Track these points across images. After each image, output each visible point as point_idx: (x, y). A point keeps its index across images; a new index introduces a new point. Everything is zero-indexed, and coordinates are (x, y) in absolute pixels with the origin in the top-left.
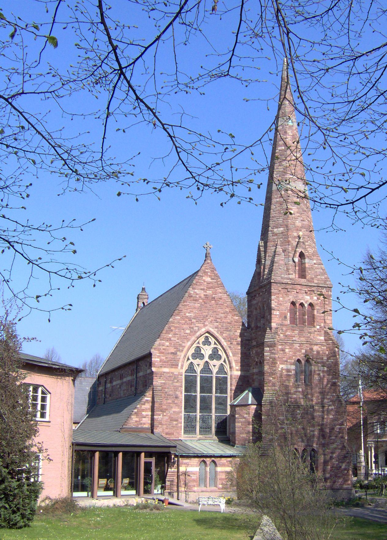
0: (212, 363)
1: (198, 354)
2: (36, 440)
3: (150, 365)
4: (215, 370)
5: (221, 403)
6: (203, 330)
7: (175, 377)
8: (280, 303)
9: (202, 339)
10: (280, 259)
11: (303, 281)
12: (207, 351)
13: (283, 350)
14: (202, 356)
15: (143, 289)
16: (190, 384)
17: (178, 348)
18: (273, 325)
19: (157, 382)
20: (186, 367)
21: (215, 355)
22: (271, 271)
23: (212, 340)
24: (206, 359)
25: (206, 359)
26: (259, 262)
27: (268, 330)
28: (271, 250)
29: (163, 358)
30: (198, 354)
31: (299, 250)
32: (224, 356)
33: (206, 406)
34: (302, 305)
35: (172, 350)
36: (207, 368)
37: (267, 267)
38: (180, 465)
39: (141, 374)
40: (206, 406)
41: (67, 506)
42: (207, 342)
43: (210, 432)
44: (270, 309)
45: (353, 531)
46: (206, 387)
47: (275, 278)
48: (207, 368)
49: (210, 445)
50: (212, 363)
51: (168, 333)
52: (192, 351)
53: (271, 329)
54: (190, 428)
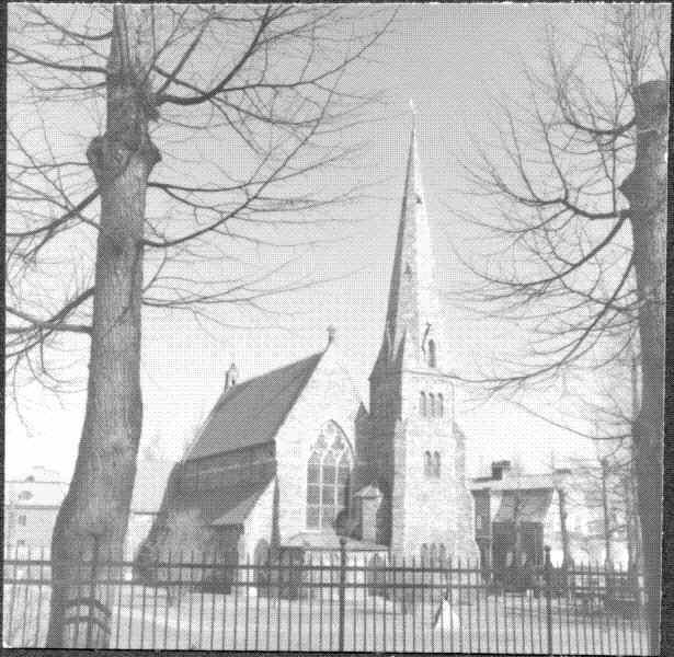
2: (96, 133)
3: (272, 454)
4: (338, 460)
8: (410, 391)
10: (409, 347)
11: (432, 371)
13: (412, 441)
15: (233, 365)
18: (404, 416)
19: (280, 472)
25: (329, 448)
28: (398, 337)
29: (530, 292)
34: (431, 395)
37: (395, 353)
38: (603, 523)
39: (257, 463)
43: (316, 524)
44: (399, 398)
45: (491, 560)
53: (400, 419)
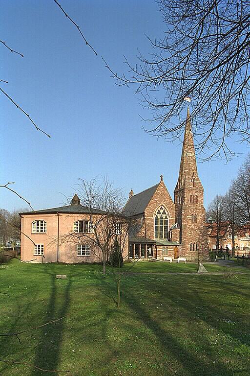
0: (163, 215)
1: (159, 213)
4: (164, 218)
5: (166, 228)
6: (161, 204)
7: (153, 220)
9: (160, 207)
12: (162, 211)
14: (160, 213)
16: (156, 222)
17: (153, 210)
20: (155, 217)
21: (164, 213)
22: (184, 185)
23: (163, 208)
24: (161, 214)
25: (161, 214)
26: (179, 181)
27: (137, 315)
30: (159, 213)
31: (193, 178)
32: (167, 213)
33: (161, 230)
35: (151, 211)
36: (161, 217)
40: (161, 230)
41: (129, 261)
42: (161, 209)
46: (161, 221)
47: (186, 187)
48: (161, 217)
49: (164, 241)
50: (163, 215)
51: (150, 205)
52: (157, 211)
54: (156, 237)
